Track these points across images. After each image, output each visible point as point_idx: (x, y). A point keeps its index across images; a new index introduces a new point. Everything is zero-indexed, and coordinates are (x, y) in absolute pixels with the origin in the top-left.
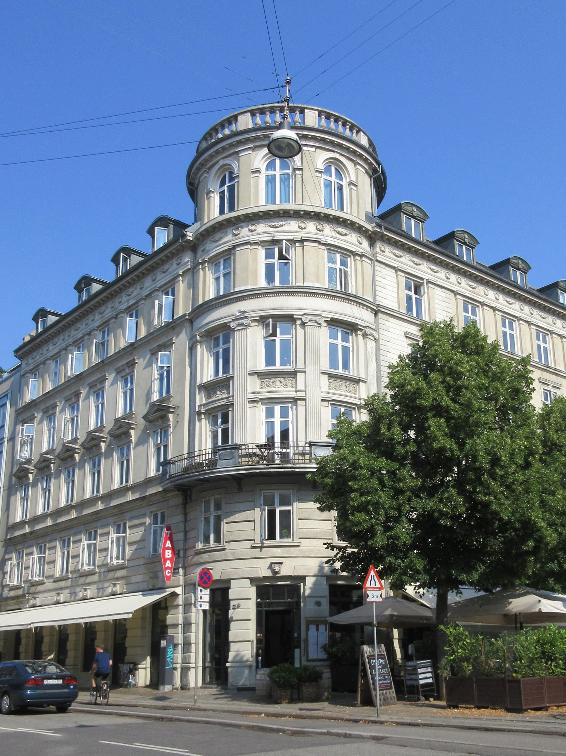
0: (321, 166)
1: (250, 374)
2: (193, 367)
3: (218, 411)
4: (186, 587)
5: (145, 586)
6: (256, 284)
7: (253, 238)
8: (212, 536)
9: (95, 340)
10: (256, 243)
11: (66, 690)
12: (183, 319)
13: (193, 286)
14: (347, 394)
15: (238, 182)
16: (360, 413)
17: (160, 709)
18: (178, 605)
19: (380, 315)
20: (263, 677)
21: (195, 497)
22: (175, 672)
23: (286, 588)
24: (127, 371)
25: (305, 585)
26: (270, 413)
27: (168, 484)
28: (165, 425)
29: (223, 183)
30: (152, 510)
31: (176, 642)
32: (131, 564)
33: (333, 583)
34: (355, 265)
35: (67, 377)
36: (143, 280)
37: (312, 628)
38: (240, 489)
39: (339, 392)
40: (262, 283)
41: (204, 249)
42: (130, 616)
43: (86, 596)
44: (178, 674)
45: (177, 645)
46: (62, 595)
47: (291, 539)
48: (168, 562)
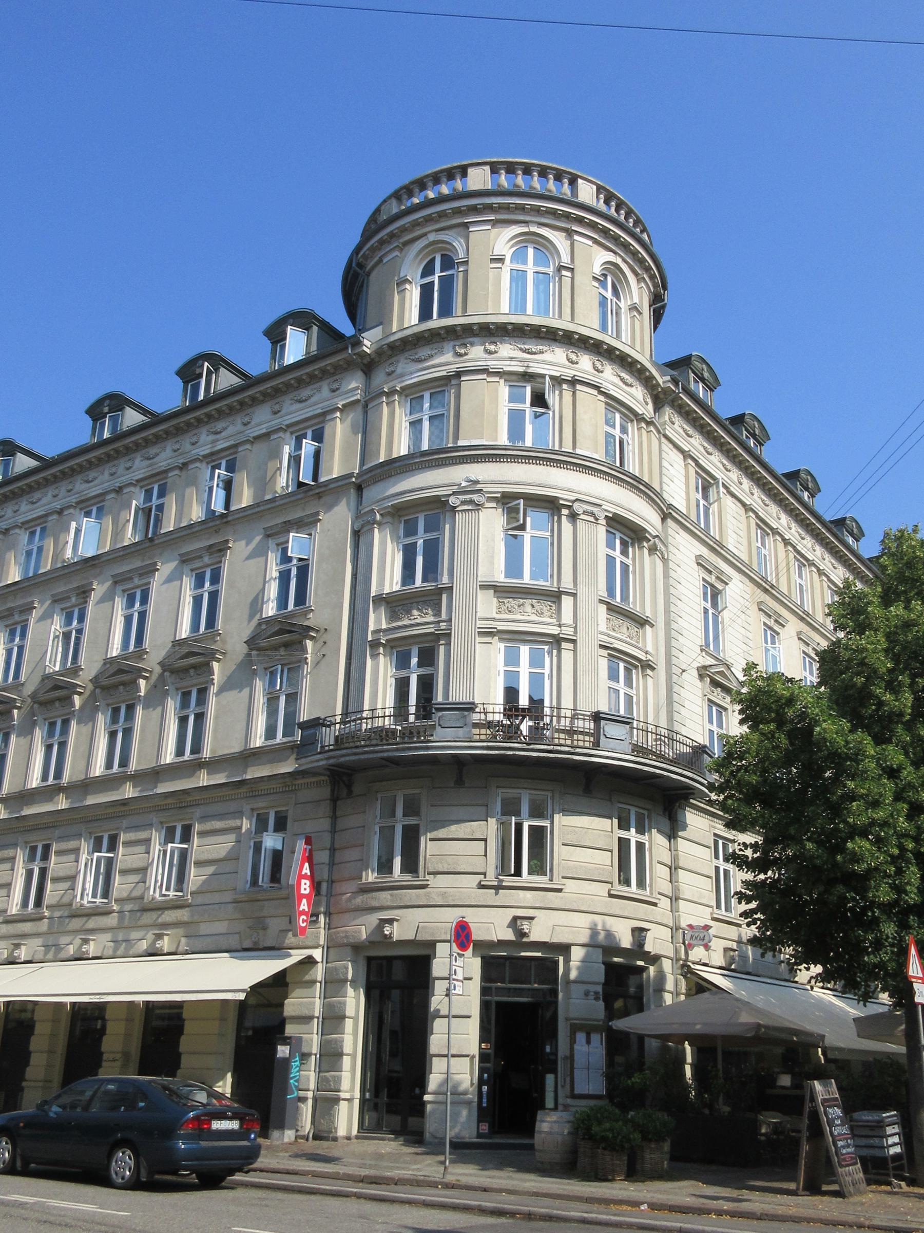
0: (597, 270)
1: (484, 587)
2: (361, 563)
3: (411, 644)
4: (331, 950)
5: (234, 942)
6: (496, 441)
7: (493, 364)
8: (397, 862)
9: (134, 502)
10: (497, 374)
11: (245, 1143)
12: (347, 481)
13: (367, 430)
14: (628, 640)
15: (466, 272)
16: (644, 676)
17: (362, 1181)
18: (314, 982)
19: (670, 522)
20: (556, 1128)
21: (377, 785)
22: (301, 1105)
23: (507, 963)
24: (206, 560)
25: (567, 961)
26: (512, 659)
27: (318, 761)
28: (294, 659)
29: (428, 270)
30: (256, 805)
31: (305, 1050)
32: (200, 900)
33: (608, 960)
34: (640, 436)
35: (60, 560)
36: (250, 410)
37: (581, 1037)
38: (459, 782)
39: (618, 635)
40: (503, 439)
41: (393, 372)
42: (242, 996)
43: (87, 952)
44: (306, 1110)
45: (310, 1055)
46: (23, 948)
47: (547, 878)
48: (304, 901)
